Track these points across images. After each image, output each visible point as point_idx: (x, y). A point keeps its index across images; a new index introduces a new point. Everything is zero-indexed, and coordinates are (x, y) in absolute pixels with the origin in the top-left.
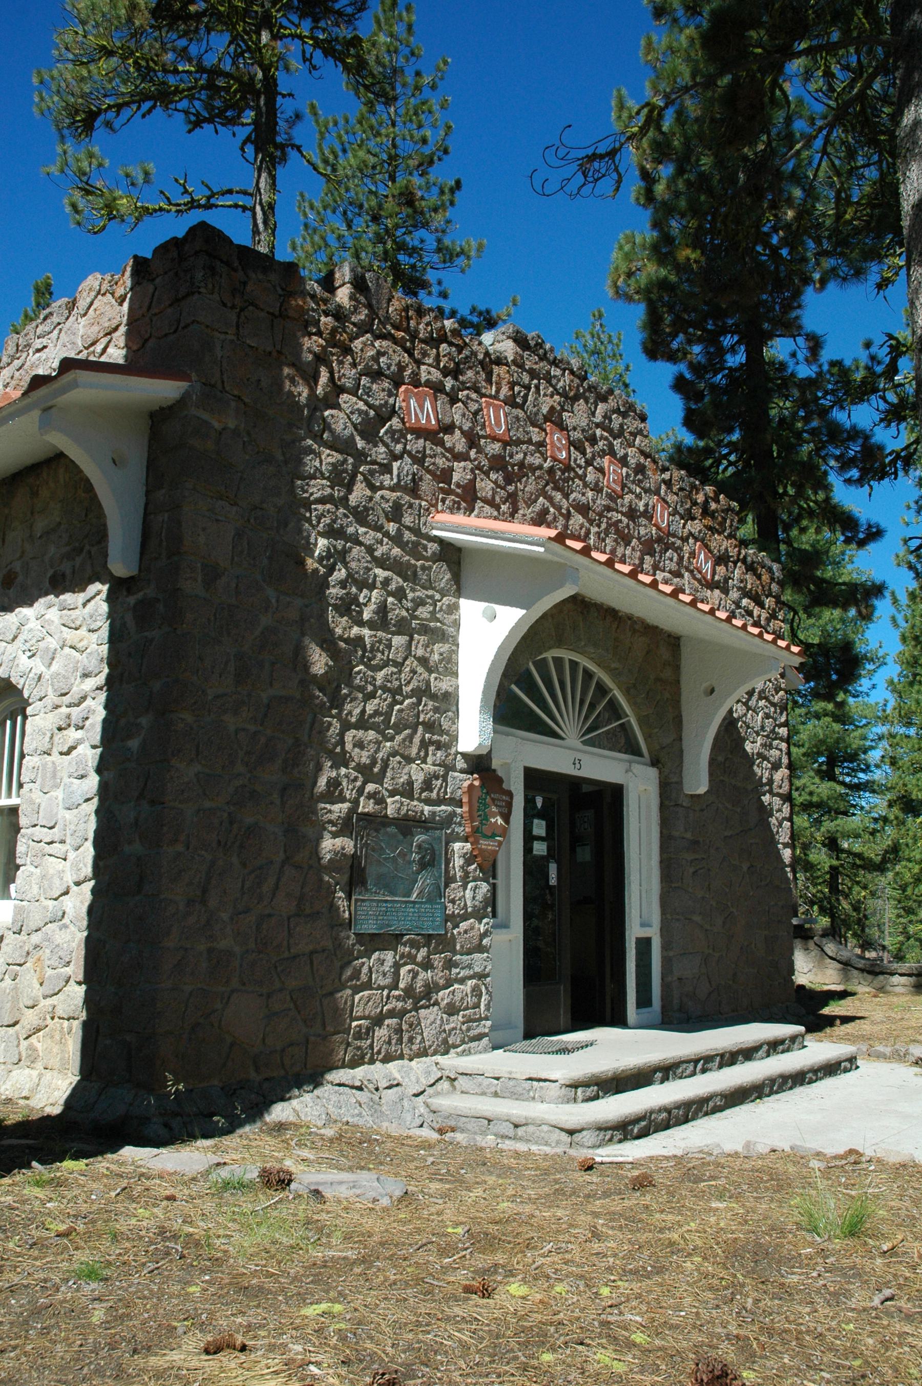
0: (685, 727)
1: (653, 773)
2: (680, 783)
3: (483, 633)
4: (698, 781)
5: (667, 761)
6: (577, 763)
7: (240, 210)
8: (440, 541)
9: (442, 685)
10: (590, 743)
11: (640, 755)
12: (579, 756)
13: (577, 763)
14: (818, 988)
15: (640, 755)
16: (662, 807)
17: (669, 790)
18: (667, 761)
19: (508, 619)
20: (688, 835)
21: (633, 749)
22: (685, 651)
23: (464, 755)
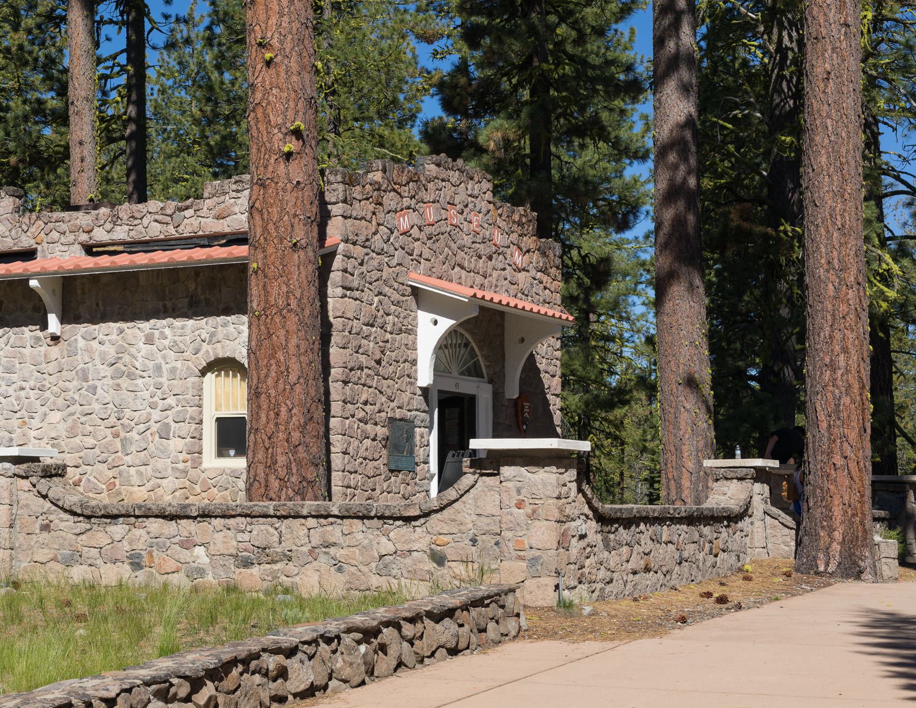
0: (507, 360)
1: (489, 387)
2: (503, 392)
3: (430, 330)
4: (513, 391)
5: (497, 380)
6: (457, 385)
7: (411, 211)
8: (411, 286)
9: (411, 355)
10: (462, 374)
11: (483, 377)
12: (457, 381)
13: (457, 385)
14: (86, 325)
15: (483, 377)
16: (494, 406)
17: (497, 395)
18: (497, 380)
19: (446, 324)
20: (507, 422)
21: (479, 374)
22: (507, 318)
23: (421, 388)
